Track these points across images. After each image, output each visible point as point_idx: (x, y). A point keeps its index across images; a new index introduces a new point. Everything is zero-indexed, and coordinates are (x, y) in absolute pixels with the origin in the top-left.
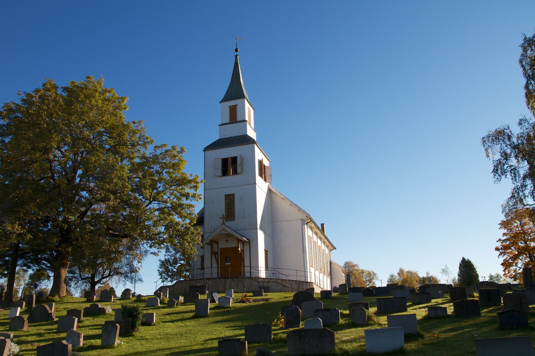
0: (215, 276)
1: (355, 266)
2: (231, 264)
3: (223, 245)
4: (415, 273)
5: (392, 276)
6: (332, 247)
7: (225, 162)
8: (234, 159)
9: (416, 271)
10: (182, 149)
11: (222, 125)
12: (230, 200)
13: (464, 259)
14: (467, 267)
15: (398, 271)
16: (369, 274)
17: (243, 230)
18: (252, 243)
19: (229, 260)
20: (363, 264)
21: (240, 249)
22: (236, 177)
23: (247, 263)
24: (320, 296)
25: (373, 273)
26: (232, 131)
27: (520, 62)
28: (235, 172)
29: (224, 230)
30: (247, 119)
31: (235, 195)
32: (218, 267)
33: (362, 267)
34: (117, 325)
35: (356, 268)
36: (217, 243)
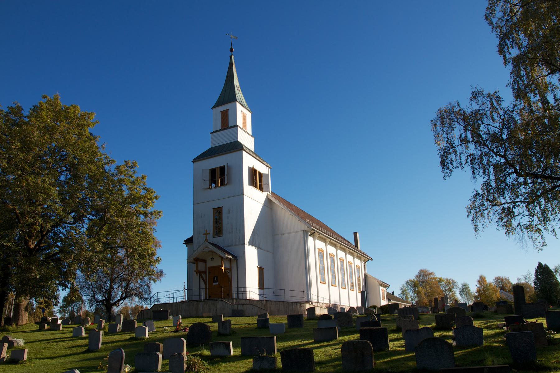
0: (203, 298)
1: (430, 274)
2: (219, 284)
3: (210, 264)
4: (506, 279)
5: (465, 285)
6: (365, 258)
7: (213, 172)
8: (222, 169)
9: (507, 277)
10: (134, 165)
11: (214, 132)
12: (218, 212)
13: (540, 264)
14: (393, 292)
15: (478, 278)
16: (448, 282)
17: (231, 246)
18: (238, 260)
19: (217, 279)
20: (441, 271)
21: (223, 268)
22: (224, 188)
23: (234, 284)
24: (256, 326)
25: (453, 281)
26: (223, 139)
27: (487, 18)
28: (222, 184)
29: (206, 247)
30: (239, 122)
31: (223, 208)
32: (206, 288)
33: (438, 275)
34: (182, 339)
35: (432, 276)
36: (204, 261)
